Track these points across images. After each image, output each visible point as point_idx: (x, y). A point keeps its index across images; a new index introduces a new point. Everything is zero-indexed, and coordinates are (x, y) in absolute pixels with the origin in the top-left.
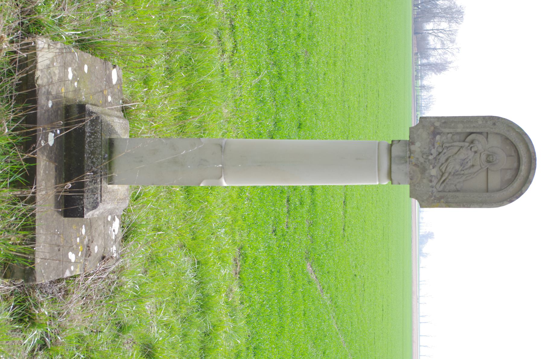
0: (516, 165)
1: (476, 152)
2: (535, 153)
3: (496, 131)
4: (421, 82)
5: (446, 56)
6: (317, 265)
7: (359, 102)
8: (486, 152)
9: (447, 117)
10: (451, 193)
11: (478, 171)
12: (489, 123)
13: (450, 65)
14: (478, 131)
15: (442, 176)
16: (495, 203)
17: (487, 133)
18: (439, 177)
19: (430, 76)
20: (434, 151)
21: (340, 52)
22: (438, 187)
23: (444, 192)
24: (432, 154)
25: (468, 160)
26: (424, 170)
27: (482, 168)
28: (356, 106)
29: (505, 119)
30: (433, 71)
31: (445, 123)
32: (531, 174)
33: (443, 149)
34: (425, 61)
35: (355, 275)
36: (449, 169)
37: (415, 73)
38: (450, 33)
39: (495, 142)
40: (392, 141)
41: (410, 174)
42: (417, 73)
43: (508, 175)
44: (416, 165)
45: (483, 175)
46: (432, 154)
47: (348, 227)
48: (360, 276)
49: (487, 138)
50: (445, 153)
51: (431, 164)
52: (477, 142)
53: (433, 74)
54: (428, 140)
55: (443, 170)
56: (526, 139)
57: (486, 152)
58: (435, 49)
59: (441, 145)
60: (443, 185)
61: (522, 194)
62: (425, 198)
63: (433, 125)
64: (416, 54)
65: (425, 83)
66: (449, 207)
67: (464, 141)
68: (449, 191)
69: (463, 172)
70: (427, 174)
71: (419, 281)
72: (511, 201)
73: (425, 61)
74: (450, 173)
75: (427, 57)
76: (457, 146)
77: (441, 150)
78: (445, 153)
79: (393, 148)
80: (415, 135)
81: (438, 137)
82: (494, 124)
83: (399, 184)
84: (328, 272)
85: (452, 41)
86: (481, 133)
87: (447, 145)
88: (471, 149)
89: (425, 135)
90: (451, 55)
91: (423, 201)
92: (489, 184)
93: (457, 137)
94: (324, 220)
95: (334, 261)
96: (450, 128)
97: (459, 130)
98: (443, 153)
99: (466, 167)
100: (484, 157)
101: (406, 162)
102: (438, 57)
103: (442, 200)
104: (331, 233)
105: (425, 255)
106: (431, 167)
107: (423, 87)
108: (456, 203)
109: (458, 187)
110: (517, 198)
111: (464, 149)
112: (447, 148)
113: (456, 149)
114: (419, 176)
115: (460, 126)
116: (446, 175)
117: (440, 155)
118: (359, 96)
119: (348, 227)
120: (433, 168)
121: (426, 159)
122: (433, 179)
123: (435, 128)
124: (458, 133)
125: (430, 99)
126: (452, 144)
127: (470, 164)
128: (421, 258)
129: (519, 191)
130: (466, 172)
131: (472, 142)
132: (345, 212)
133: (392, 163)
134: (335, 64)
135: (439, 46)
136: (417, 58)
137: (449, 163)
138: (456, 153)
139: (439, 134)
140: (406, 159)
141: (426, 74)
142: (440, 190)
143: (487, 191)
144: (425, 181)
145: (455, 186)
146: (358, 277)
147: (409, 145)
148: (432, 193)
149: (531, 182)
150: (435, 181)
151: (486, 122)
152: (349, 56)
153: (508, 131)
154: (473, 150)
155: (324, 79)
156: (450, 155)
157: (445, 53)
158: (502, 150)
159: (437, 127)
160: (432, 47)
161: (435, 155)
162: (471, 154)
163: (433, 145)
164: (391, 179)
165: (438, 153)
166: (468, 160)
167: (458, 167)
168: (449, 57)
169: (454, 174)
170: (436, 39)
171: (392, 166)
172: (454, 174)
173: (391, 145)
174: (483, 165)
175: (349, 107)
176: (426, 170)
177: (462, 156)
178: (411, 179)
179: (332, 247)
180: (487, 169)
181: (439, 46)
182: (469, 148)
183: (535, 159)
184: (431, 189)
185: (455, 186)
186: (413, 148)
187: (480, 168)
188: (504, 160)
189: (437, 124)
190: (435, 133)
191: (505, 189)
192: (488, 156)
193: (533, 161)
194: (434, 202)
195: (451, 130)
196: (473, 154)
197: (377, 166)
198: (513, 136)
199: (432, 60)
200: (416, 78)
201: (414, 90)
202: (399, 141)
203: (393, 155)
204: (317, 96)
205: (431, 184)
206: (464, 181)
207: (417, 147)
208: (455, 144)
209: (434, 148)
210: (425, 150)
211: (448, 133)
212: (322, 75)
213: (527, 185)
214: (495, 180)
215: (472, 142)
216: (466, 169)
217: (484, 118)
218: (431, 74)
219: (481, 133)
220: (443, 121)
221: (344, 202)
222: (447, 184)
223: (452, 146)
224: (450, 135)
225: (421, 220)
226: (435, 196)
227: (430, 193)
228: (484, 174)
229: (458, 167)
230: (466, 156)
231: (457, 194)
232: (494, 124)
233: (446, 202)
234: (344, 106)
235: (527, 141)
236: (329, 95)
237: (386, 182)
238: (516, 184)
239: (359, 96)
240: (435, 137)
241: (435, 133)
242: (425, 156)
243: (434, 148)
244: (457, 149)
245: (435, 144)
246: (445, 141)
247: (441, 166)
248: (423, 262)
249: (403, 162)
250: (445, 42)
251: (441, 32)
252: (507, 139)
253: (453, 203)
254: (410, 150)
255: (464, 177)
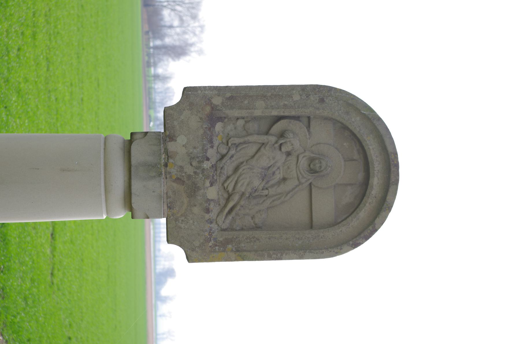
0: (361, 176)
1: (289, 154)
2: (396, 154)
3: (326, 114)
4: (155, 70)
5: (187, 36)
6: (10, 332)
7: (71, 93)
8: (307, 154)
9: (236, 87)
10: (245, 233)
11: (293, 189)
12: (312, 98)
13: (192, 49)
14: (293, 113)
15: (228, 200)
16: (327, 249)
17: (309, 118)
18: (222, 202)
19: (166, 63)
20: (211, 153)
21: (42, 20)
22: (220, 222)
23: (233, 230)
24: (208, 159)
25: (274, 169)
26: (193, 190)
27: (300, 183)
28: (67, 98)
29: (340, 90)
30: (170, 55)
31: (231, 98)
32: (390, 194)
33: (229, 148)
34: (158, 43)
35: (70, 338)
36: (241, 188)
37: (146, 58)
38: (191, 5)
39: (323, 135)
40: (132, 134)
41: (168, 197)
42: (149, 58)
43: (348, 196)
44: (178, 180)
45: (302, 197)
46: (208, 159)
47: (59, 270)
48: (77, 338)
49: (309, 127)
50: (232, 156)
51: (207, 177)
52: (291, 135)
53: (170, 60)
54: (201, 132)
55: (230, 189)
56: (380, 128)
57: (307, 154)
58: (171, 27)
59: (224, 141)
60: (230, 217)
61: (375, 230)
62: (197, 243)
63: (209, 102)
64: (147, 33)
65: (160, 71)
66: (243, 259)
67: (267, 133)
68: (242, 229)
69: (266, 192)
70: (199, 198)
71: (157, 334)
72: (356, 245)
73: (158, 43)
74: (243, 194)
75: (162, 37)
76: (255, 142)
77: (224, 151)
78: (232, 156)
79: (134, 147)
80: (176, 123)
81: (219, 126)
82: (322, 101)
83: (148, 218)
84: (29, 340)
85: (194, 17)
86: (297, 118)
87: (237, 141)
88: (280, 149)
89: (194, 120)
90: (192, 35)
91: (193, 250)
92: (314, 214)
93: (253, 126)
94: (22, 263)
95: (37, 321)
96: (241, 108)
97: (258, 113)
98: (229, 155)
99: (271, 183)
100: (303, 162)
101: (160, 174)
102: (176, 37)
103: (230, 246)
104: (32, 280)
105: (164, 300)
106: (208, 184)
107: (157, 77)
108: (256, 251)
109: (257, 220)
110: (367, 238)
111: (267, 148)
112: (237, 146)
113: (253, 149)
114: (186, 200)
115: (260, 104)
116: (236, 198)
117: (224, 161)
118: (71, 85)
119: (59, 270)
120: (212, 185)
121: (197, 168)
122: (212, 206)
123: (212, 108)
124: (255, 119)
125: (166, 93)
126: (246, 139)
127: (278, 176)
128: (159, 303)
129: (368, 226)
130: (272, 191)
131: (282, 135)
132: (53, 249)
133: (133, 177)
134: (34, 36)
135: (176, 23)
136: (149, 39)
137: (241, 175)
138: (253, 157)
139: (220, 119)
140: (159, 168)
141: (160, 60)
142: (224, 226)
143: (311, 227)
144: (196, 210)
145: (253, 217)
146: (74, 340)
147: (165, 141)
148: (210, 234)
149: (390, 209)
150: (215, 209)
151: (308, 96)
152: (56, 27)
153: (347, 113)
154: (283, 149)
155: (18, 56)
156: (241, 160)
157: (185, 33)
158: (337, 149)
159: (217, 106)
160: (168, 24)
161: (213, 160)
162: (280, 157)
163: (211, 141)
164: (131, 209)
165: (219, 156)
166: (274, 169)
167: (257, 183)
168: (190, 38)
169: (251, 196)
170: (173, 13)
171: (133, 182)
172: (251, 196)
173: (131, 142)
174: (303, 177)
175: (56, 99)
176: (199, 189)
177: (264, 162)
178: (169, 208)
179: (33, 302)
180: (310, 184)
181: (176, 23)
182: (277, 145)
183: (397, 166)
184: (207, 226)
185: (253, 217)
186: (171, 146)
187: (296, 182)
188: (340, 169)
189: (217, 101)
190: (213, 118)
191: (344, 222)
192: (311, 160)
193: (393, 169)
194: (215, 251)
195: (244, 113)
196: (284, 157)
197: (103, 184)
198: (355, 123)
199: (168, 41)
200: (148, 65)
201: (146, 81)
202: (146, 133)
203: (134, 161)
204: (7, 81)
205: (207, 216)
206: (268, 208)
207: (179, 146)
208: (251, 138)
209: (212, 147)
210: (195, 151)
211: (238, 119)
212: (15, 51)
213: (383, 213)
214: (325, 206)
215: (282, 135)
216: (272, 186)
217: (303, 88)
218: (167, 60)
219: (297, 118)
220: (228, 95)
221: (52, 235)
222: (237, 214)
223: (245, 143)
224: (241, 122)
225: (157, 253)
226: (215, 239)
227: (207, 234)
228: (305, 194)
229: (257, 183)
230: (272, 162)
231: (257, 234)
232: (322, 101)
233: (238, 251)
234: (49, 98)
235: (383, 132)
236: (26, 80)
237: (122, 215)
238: (363, 213)
239: (71, 85)
240: (213, 126)
241: (213, 118)
242: (194, 163)
243: (212, 147)
244: (254, 148)
245: (215, 138)
246: (231, 133)
247: (225, 181)
248: (163, 308)
249: (154, 174)
250: (184, 18)
251: (179, 5)
252: (345, 128)
253: (250, 251)
254: (166, 152)
255: (269, 201)
